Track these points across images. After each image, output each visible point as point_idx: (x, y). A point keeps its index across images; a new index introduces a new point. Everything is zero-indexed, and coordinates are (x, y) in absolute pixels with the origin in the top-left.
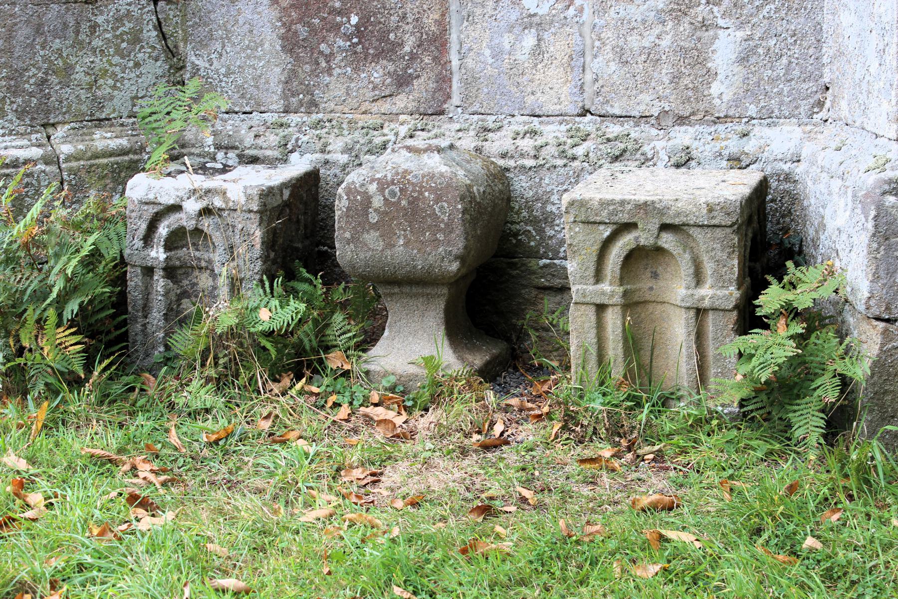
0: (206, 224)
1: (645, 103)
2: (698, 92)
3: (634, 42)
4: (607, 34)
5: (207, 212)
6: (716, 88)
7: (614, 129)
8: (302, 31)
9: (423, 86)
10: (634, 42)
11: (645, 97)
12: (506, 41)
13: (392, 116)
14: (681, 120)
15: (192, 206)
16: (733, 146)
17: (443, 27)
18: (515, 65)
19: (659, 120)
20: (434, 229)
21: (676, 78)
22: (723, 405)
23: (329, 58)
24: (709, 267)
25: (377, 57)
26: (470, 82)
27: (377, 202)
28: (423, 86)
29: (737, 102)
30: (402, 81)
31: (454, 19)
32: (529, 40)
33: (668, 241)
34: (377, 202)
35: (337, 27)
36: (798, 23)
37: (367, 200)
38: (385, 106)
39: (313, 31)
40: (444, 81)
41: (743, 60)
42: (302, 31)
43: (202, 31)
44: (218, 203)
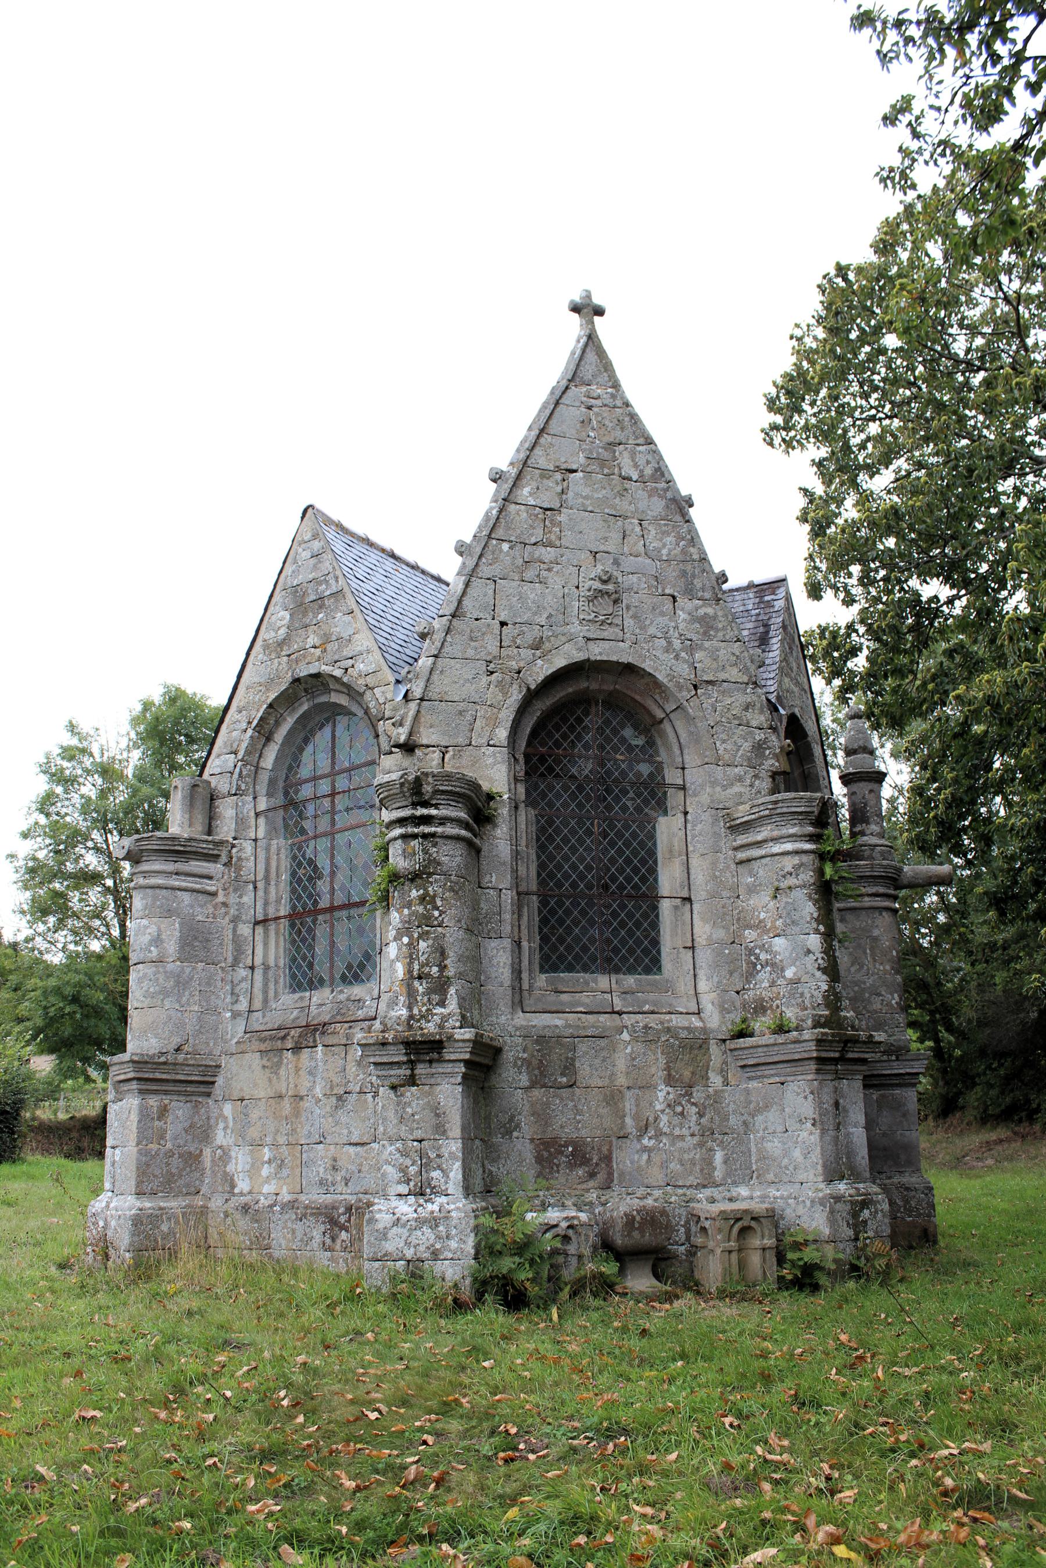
0: (571, 1232)
1: (692, 1180)
2: (711, 1175)
3: (686, 1156)
4: (676, 1154)
5: (569, 1227)
6: (716, 1173)
7: (680, 1191)
8: (545, 1154)
9: (601, 1177)
10: (686, 1156)
11: (691, 1178)
12: (636, 1157)
13: (588, 1190)
14: (704, 1186)
15: (564, 1224)
16: (728, 1195)
17: (610, 1151)
18: (639, 1167)
19: (696, 1187)
20: (661, 1228)
21: (702, 1170)
22: (123, 1560)
23: (558, 1166)
24: (767, 1232)
25: (580, 1165)
26: (622, 1174)
27: (638, 1218)
28: (601, 1177)
29: (724, 1179)
30: (592, 1175)
31: (614, 1148)
32: (645, 1157)
33: (753, 1224)
34: (638, 1218)
35: (562, 1153)
36: (743, 1148)
37: (634, 1217)
38: (584, 1186)
39: (551, 1154)
40: (610, 1174)
41: (725, 1162)
42: (545, 1154)
43: (494, 1155)
44: (576, 1222)
